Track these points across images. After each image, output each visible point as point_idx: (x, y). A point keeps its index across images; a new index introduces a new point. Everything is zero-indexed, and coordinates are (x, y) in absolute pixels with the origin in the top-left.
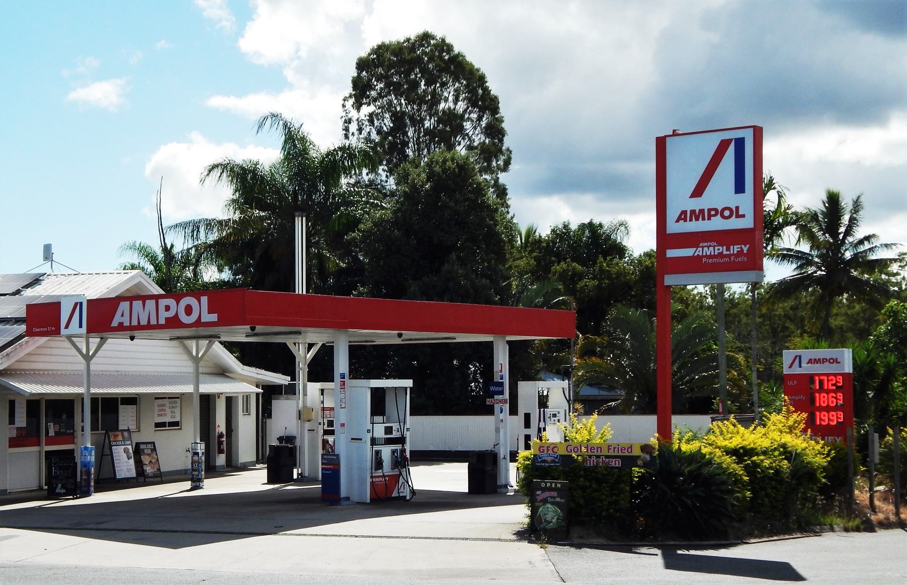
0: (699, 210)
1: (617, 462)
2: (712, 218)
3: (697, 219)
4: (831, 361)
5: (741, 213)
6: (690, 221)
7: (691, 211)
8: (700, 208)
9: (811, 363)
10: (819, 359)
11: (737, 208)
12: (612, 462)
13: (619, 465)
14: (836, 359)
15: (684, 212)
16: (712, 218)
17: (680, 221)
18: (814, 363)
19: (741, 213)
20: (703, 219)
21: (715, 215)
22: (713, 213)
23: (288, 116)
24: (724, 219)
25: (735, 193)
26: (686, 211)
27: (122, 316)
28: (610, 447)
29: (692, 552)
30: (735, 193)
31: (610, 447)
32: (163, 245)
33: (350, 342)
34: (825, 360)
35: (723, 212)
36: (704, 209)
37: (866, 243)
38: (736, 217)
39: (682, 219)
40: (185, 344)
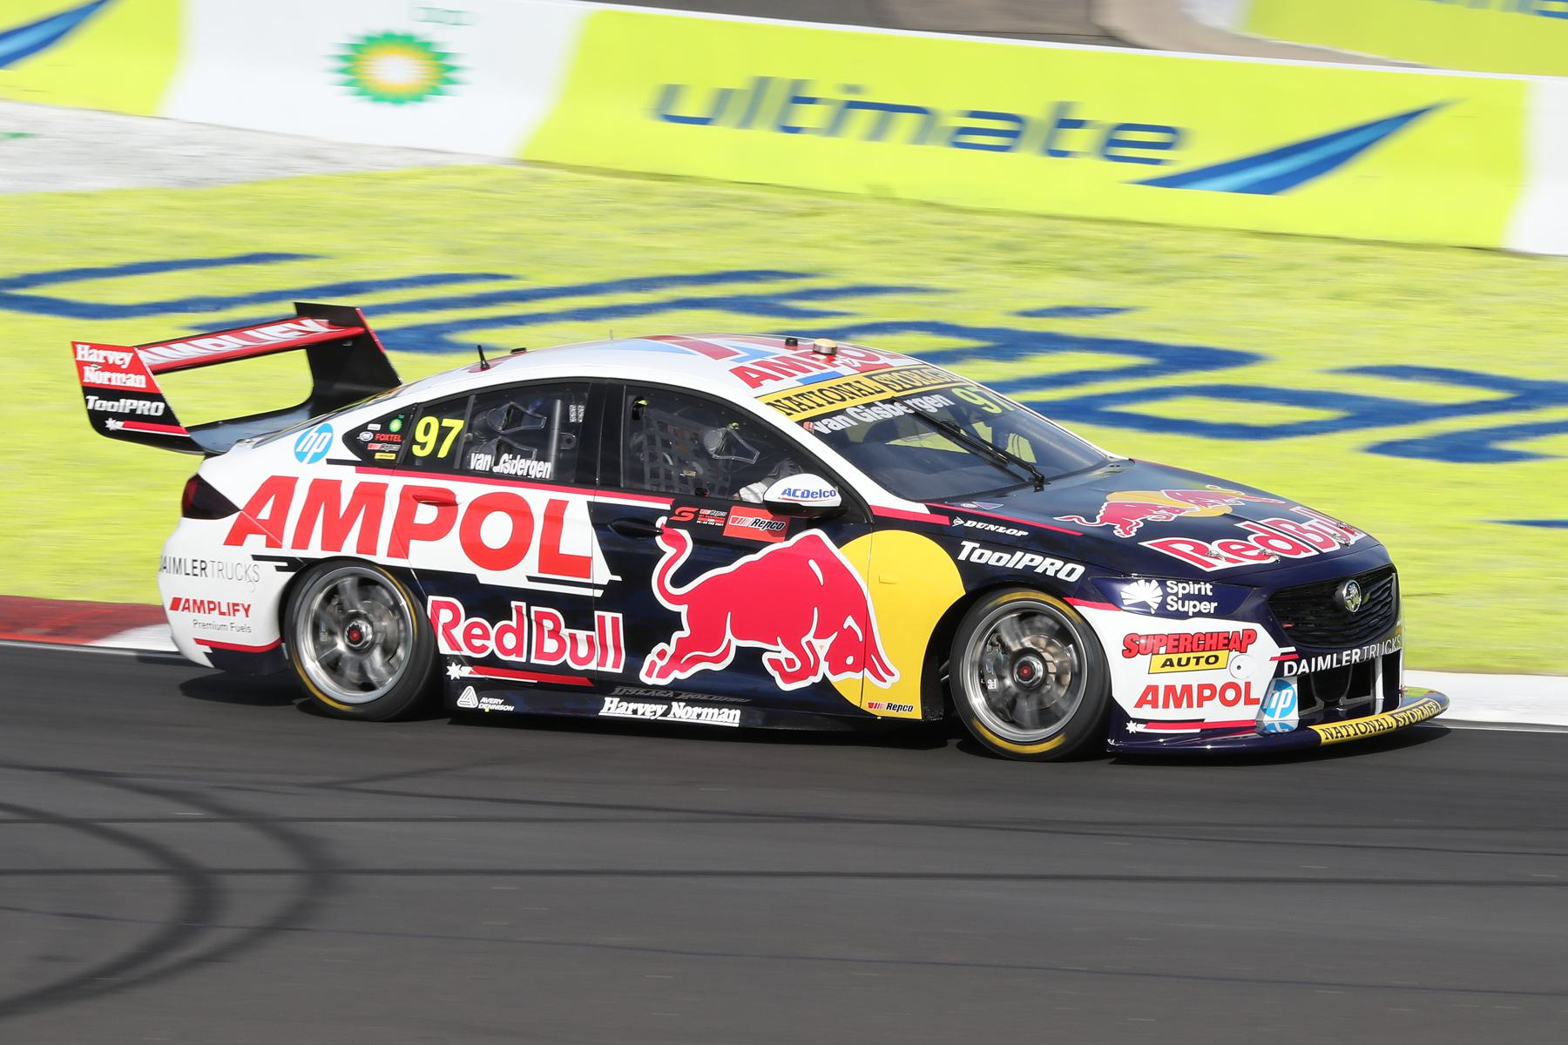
0: (1183, 686)
2: (1204, 702)
6: (180, 599)
7: (1166, 687)
9: (1154, 704)
11: (1248, 685)
12: (486, 636)
15: (1152, 689)
16: (1204, 702)
17: (1144, 706)
18: (1166, 705)
22: (1207, 693)
25: (341, 481)
26: (1191, 686)
27: (1235, 643)
28: (236, 608)
30: (341, 481)
31: (236, 608)
34: (212, 606)
36: (1191, 686)
38: (1246, 703)
39: (1148, 702)
40: (177, 645)
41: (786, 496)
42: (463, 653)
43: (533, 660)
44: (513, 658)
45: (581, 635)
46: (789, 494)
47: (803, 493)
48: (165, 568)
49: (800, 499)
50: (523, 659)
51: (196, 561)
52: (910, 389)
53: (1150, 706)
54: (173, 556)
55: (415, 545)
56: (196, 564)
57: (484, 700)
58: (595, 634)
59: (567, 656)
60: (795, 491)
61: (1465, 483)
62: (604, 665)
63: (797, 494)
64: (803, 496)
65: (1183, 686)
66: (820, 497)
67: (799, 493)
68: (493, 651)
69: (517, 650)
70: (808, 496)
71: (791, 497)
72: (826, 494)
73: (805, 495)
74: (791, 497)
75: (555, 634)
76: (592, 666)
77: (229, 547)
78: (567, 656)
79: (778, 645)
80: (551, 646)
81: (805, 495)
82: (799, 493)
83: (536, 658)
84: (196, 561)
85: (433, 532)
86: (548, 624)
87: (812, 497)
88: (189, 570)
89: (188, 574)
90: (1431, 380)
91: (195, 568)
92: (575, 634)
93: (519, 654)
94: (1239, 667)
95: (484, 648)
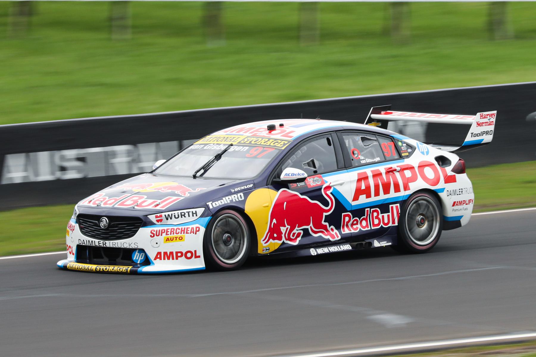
1: (386, 221)
3: (169, 259)
4: (189, 255)
5: (197, 255)
8: (170, 251)
10: (171, 253)
11: (195, 251)
13: (393, 223)
14: (472, 137)
15: (159, 253)
17: (157, 259)
18: (164, 259)
19: (197, 255)
20: (460, 201)
21: (181, 256)
23: (379, 244)
24: (191, 258)
26: (161, 252)
29: (211, 294)
32: (313, 252)
33: (457, 190)
34: (179, 254)
35: (190, 257)
36: (161, 252)
37: (160, 222)
39: (158, 258)
41: (286, 176)
42: (352, 232)
43: (373, 228)
44: (366, 229)
45: (386, 215)
46: (287, 175)
47: (292, 174)
48: (451, 194)
49: (291, 176)
50: (369, 229)
51: (460, 189)
52: (274, 141)
53: (159, 259)
54: (453, 189)
55: (411, 185)
56: (460, 190)
57: (381, 243)
58: (390, 214)
59: (382, 224)
60: (289, 174)
61: (164, 175)
62: (395, 224)
63: (290, 175)
64: (292, 175)
65: (170, 252)
66: (298, 175)
67: (290, 175)
68: (360, 229)
69: (367, 226)
70: (294, 175)
71: (288, 176)
72: (301, 175)
73: (293, 175)
74: (288, 176)
75: (377, 217)
76: (390, 224)
77: (444, 188)
78: (382, 224)
79: (102, 258)
80: (376, 222)
81: (293, 175)
82: (290, 175)
83: (373, 227)
84: (460, 189)
85: (414, 179)
86: (375, 214)
87: (295, 175)
88: (458, 194)
89: (458, 195)
90: (334, 127)
91: (460, 192)
92: (375, 217)
93: (368, 227)
94: (157, 243)
95: (357, 228)
